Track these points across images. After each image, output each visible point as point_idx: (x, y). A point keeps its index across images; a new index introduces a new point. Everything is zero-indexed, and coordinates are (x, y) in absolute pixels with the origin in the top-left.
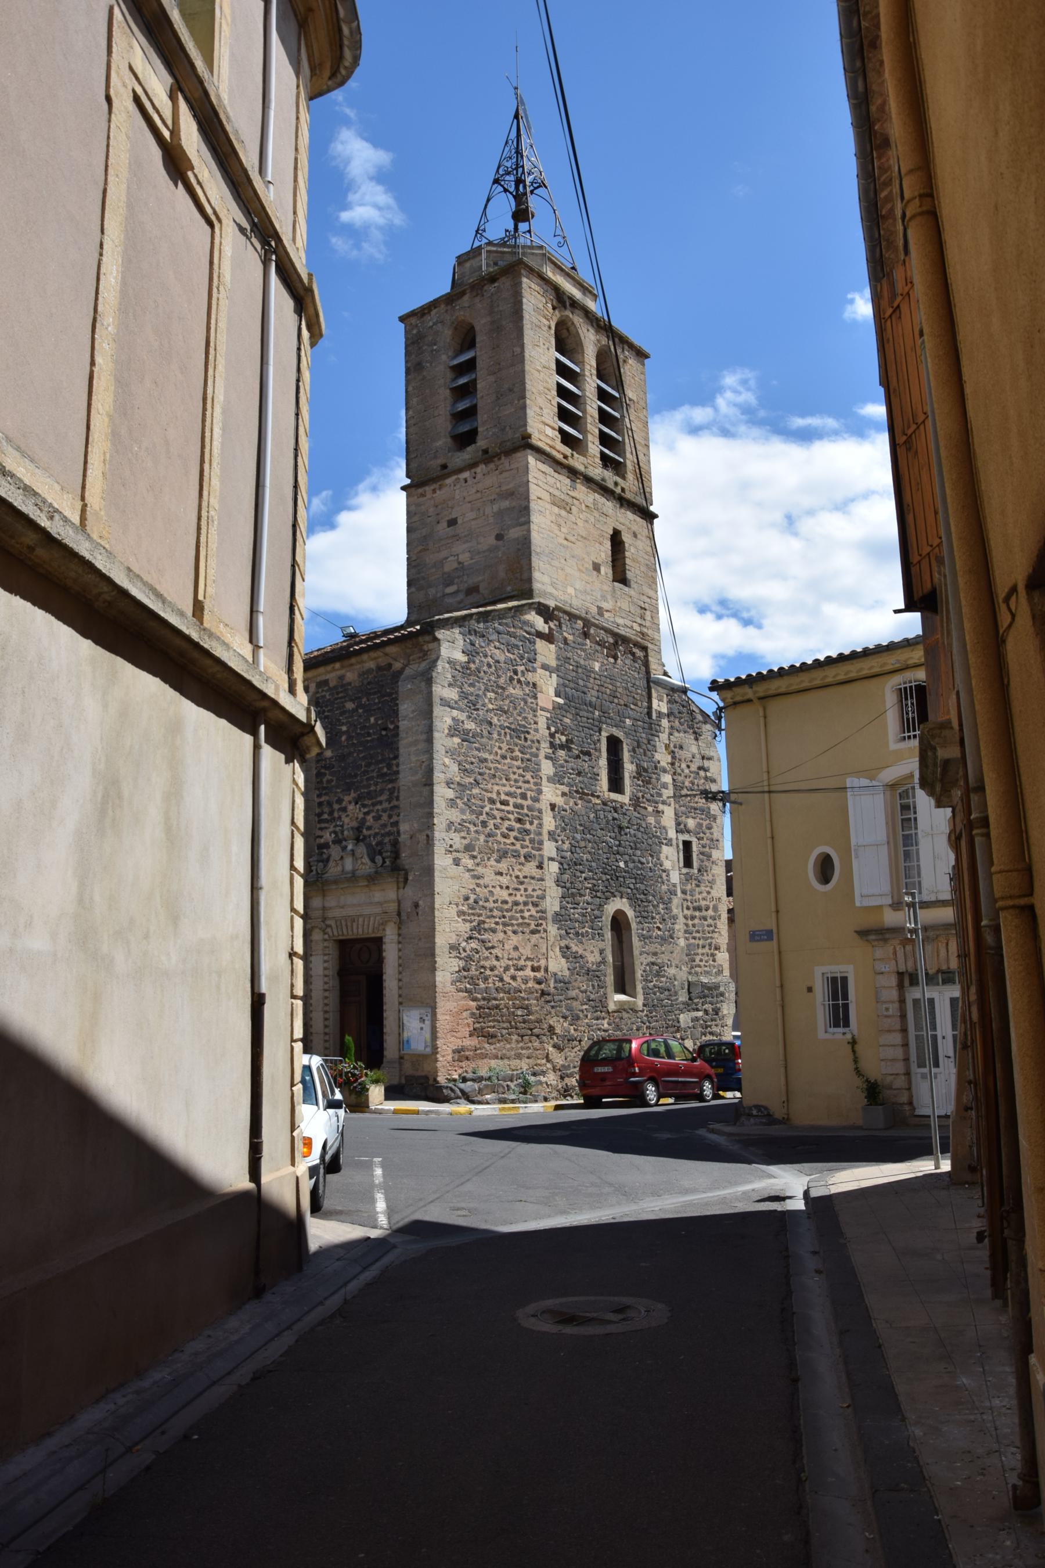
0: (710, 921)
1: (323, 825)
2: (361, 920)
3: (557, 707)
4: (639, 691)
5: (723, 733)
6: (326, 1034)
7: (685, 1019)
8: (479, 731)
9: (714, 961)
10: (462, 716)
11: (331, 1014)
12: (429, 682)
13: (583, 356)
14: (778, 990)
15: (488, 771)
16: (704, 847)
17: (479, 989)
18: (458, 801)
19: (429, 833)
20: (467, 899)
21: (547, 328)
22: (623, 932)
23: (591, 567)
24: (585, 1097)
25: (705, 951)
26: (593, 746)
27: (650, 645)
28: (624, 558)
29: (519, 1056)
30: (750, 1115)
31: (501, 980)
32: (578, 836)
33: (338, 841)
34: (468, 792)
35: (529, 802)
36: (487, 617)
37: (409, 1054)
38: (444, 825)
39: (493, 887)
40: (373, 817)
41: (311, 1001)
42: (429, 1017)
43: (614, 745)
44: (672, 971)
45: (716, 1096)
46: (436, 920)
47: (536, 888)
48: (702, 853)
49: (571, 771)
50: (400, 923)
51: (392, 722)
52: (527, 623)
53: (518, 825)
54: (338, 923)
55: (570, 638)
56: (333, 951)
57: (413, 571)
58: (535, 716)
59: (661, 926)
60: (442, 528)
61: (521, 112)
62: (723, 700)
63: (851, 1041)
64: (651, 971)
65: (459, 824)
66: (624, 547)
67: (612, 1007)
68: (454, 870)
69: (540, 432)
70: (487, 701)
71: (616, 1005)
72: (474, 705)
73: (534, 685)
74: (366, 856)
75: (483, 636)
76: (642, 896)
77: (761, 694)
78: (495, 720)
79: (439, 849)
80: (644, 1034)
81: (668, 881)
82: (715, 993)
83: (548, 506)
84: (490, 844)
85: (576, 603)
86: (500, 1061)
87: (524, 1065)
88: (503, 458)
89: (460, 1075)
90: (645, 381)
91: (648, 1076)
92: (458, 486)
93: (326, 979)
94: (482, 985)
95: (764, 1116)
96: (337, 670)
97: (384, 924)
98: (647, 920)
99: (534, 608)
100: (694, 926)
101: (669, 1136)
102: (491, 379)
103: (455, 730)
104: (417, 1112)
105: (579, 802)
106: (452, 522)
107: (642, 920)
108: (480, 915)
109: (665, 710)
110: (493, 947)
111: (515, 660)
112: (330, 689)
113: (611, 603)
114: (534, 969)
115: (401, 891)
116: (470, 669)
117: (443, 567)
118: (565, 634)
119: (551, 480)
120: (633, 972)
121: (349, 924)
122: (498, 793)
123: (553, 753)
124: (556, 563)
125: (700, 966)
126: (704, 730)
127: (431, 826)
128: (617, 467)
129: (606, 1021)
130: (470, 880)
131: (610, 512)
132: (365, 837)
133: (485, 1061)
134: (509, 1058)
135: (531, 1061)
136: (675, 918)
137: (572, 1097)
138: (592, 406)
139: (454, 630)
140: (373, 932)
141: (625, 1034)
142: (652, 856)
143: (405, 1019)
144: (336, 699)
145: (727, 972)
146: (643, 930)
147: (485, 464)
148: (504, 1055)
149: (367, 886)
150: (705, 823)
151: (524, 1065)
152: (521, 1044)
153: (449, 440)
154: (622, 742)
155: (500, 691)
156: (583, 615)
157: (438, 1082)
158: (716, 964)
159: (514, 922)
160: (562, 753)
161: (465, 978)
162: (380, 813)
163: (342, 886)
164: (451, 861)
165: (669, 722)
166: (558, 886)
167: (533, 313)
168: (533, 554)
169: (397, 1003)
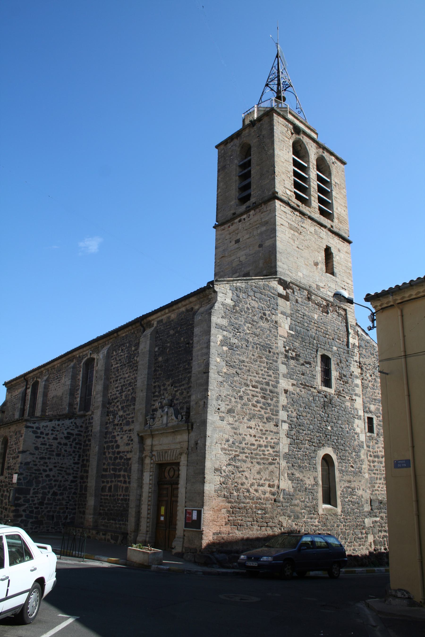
2: (169, 452)
4: (342, 333)
7: (368, 522)
10: (230, 335)
11: (152, 506)
12: (210, 314)
15: (245, 368)
18: (225, 383)
20: (228, 441)
23: (313, 264)
25: (380, 482)
26: (313, 360)
27: (348, 308)
28: (333, 261)
30: (396, 597)
31: (248, 491)
32: (301, 409)
33: (162, 407)
35: (271, 387)
39: (245, 435)
40: (179, 393)
43: (326, 360)
44: (360, 492)
47: (274, 437)
49: (299, 372)
53: (263, 400)
54: (159, 454)
55: (300, 300)
57: (218, 268)
59: (353, 465)
62: (375, 307)
64: (347, 491)
67: (321, 512)
70: (246, 328)
73: (276, 322)
74: (173, 415)
75: (245, 292)
76: (342, 447)
77: (399, 301)
78: (251, 340)
79: (211, 410)
81: (359, 439)
83: (288, 230)
84: (244, 410)
85: (303, 281)
88: (263, 206)
95: (406, 598)
96: (167, 313)
97: (181, 454)
98: (344, 461)
100: (374, 466)
103: (224, 342)
105: (303, 390)
108: (236, 451)
110: (243, 471)
114: (269, 486)
121: (163, 454)
125: (378, 490)
129: (317, 520)
131: (324, 237)
136: (362, 461)
138: (314, 184)
140: (175, 460)
144: (166, 329)
153: (237, 201)
154: (330, 359)
160: (292, 362)
162: (183, 391)
164: (218, 418)
168: (277, 253)
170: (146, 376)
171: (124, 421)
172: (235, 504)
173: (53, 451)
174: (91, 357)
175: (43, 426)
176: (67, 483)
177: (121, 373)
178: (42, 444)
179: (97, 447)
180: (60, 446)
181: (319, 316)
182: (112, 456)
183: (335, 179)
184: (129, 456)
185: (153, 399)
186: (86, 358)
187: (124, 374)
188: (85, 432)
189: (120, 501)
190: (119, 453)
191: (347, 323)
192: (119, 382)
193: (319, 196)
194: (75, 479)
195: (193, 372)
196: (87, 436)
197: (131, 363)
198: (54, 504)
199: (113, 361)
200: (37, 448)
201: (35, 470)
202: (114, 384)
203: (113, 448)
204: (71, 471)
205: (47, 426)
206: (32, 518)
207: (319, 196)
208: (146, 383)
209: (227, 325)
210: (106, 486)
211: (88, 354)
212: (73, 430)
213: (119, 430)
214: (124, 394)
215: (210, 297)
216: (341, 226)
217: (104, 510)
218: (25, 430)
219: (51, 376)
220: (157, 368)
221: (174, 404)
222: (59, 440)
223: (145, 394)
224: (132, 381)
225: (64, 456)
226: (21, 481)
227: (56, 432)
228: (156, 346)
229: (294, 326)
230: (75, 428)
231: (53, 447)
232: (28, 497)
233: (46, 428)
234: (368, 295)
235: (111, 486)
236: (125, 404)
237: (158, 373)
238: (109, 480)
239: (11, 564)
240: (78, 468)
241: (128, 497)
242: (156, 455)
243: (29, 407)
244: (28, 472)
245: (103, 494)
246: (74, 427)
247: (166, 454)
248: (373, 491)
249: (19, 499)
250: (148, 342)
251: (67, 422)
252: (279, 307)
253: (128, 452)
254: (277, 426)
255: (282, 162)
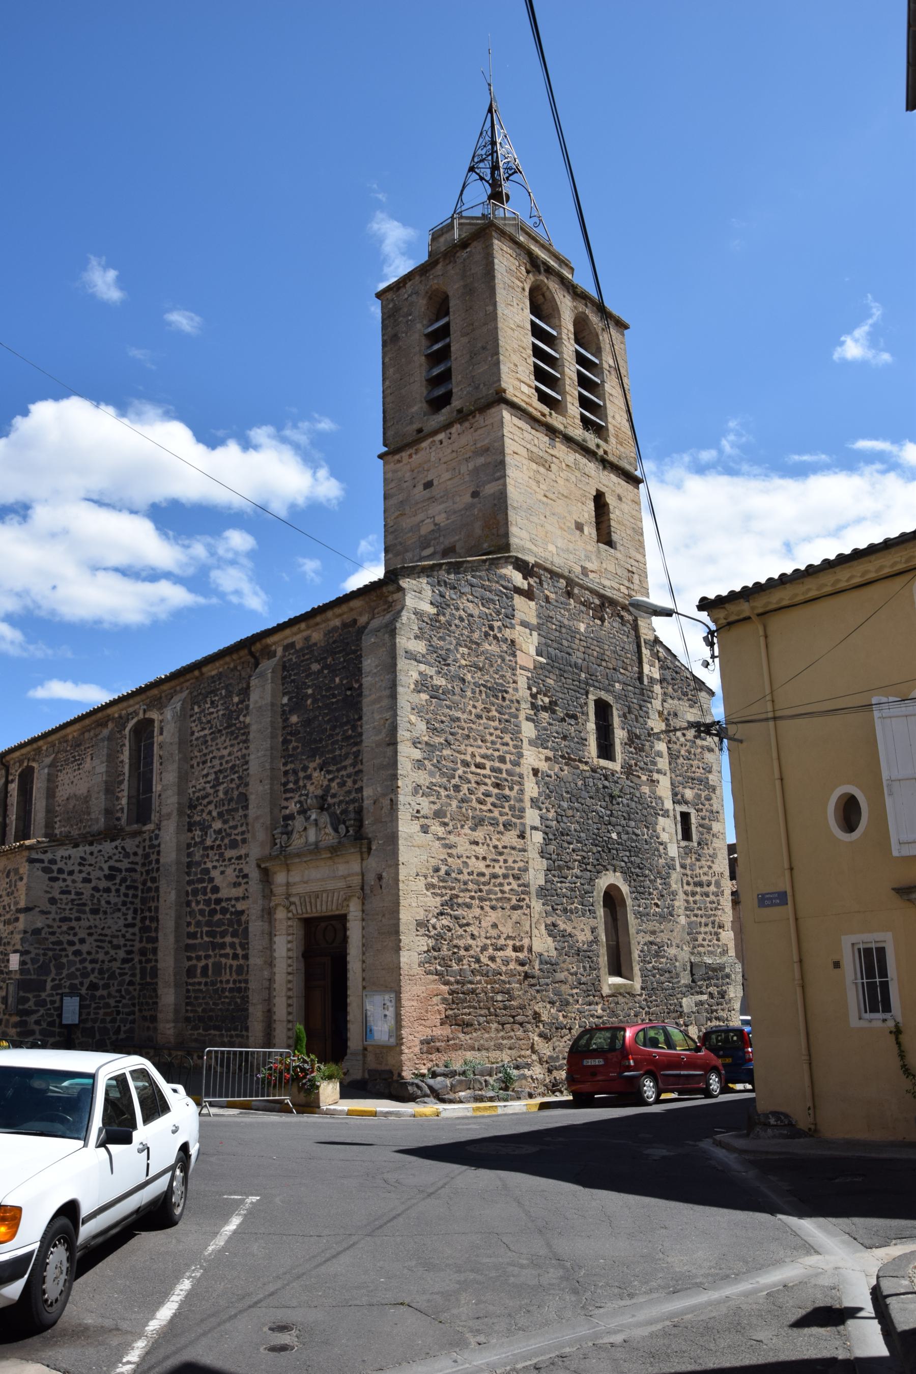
0: (712, 898)
1: (288, 795)
2: (324, 895)
3: (538, 667)
4: (629, 656)
5: (717, 660)
6: (289, 1021)
7: (688, 1003)
9: (718, 940)
10: (431, 671)
11: (295, 999)
12: (393, 633)
13: (560, 321)
14: (796, 967)
15: (460, 731)
16: (703, 819)
17: (452, 971)
18: (426, 762)
19: (393, 797)
20: (437, 870)
21: (519, 290)
22: (618, 908)
23: (573, 526)
24: (574, 1093)
25: (707, 929)
26: (579, 710)
28: (609, 520)
29: (499, 1047)
30: (767, 1125)
31: (478, 961)
32: (565, 805)
33: (303, 812)
34: (438, 753)
35: (509, 766)
36: (459, 568)
37: (373, 1046)
39: (467, 857)
40: (338, 784)
42: (393, 1004)
43: (603, 709)
44: (672, 951)
45: (725, 1090)
46: (401, 893)
47: (518, 859)
48: (702, 826)
50: (364, 898)
51: (357, 681)
52: (504, 577)
53: (496, 791)
55: (552, 596)
56: (298, 931)
57: (391, 537)
58: (514, 675)
59: (659, 903)
60: (419, 492)
61: (494, 106)
62: (714, 621)
63: (894, 1029)
64: (649, 951)
65: (428, 788)
66: (609, 508)
67: (606, 991)
68: (421, 838)
69: (515, 388)
70: (459, 656)
71: (610, 989)
72: (445, 660)
73: (513, 642)
74: (329, 826)
75: (455, 588)
76: (637, 870)
77: (760, 610)
78: (469, 677)
81: (666, 854)
82: (720, 974)
83: (526, 462)
84: (464, 810)
86: (477, 1053)
88: (478, 415)
89: (429, 1070)
90: (625, 350)
92: (434, 448)
93: (290, 961)
94: (456, 967)
95: (785, 1125)
96: (304, 630)
97: (347, 899)
99: (512, 563)
100: (695, 902)
101: (664, 1152)
102: (465, 340)
103: (422, 685)
104: (375, 1114)
105: (566, 768)
106: (428, 485)
107: (638, 896)
108: (452, 889)
109: (657, 676)
110: (468, 924)
111: (491, 615)
112: (297, 652)
113: (596, 563)
114: (516, 949)
116: (439, 621)
117: (419, 530)
120: (630, 953)
121: (313, 901)
122: (473, 755)
123: (535, 714)
125: (702, 946)
127: (395, 789)
129: (600, 1006)
130: (441, 849)
131: (593, 473)
132: (330, 806)
133: (459, 1052)
135: (513, 1052)
136: (674, 894)
137: (561, 1092)
138: (571, 370)
139: (421, 580)
140: (337, 909)
141: (621, 1021)
142: (647, 828)
143: (369, 1007)
144: (303, 661)
145: (732, 952)
146: (639, 906)
147: (460, 423)
149: (330, 858)
150: (703, 794)
151: (505, 1057)
152: (502, 1034)
153: (425, 405)
155: (474, 646)
156: (566, 574)
157: (403, 1078)
158: (720, 943)
159: (493, 897)
160: (545, 715)
161: (435, 958)
163: (305, 859)
164: (418, 828)
165: (662, 688)
166: (542, 857)
167: (505, 274)
168: (510, 508)
169: (361, 987)
170: (268, 753)
171: (226, 841)
172: (456, 986)
173: (84, 905)
174: (147, 716)
175: (62, 857)
176: (116, 965)
177: (213, 748)
178: (63, 892)
179: (173, 893)
180: (97, 895)
181: (588, 625)
182: (204, 907)
184: (240, 906)
185: (284, 796)
186: (135, 720)
187: (218, 749)
188: (144, 865)
189: (227, 994)
190: (218, 901)
191: (638, 637)
192: (209, 764)
193: (580, 394)
195: (364, 744)
196: (148, 872)
197: (233, 728)
198: (93, 1005)
199: (193, 725)
200: (53, 901)
201: (53, 943)
202: (199, 768)
203: (205, 894)
204: (122, 941)
205: (70, 857)
206: (54, 1036)
207: (580, 394)
208: (268, 766)
209: (424, 651)
210: (195, 966)
211: (139, 709)
212: (121, 861)
213: (217, 857)
214: (221, 788)
215: (390, 599)
216: (622, 449)
218: (27, 867)
220: (289, 737)
222: (93, 884)
224: (238, 762)
225: (105, 913)
226: (26, 967)
228: (284, 694)
229: (544, 648)
231: (84, 896)
233: (67, 861)
235: (207, 965)
236: (226, 808)
238: (202, 953)
239: (146, 1120)
240: (134, 934)
241: (243, 985)
242: (298, 903)
243: (17, 819)
244: (39, 948)
245: (191, 981)
248: (694, 947)
249: (26, 1000)
250: (269, 687)
251: (108, 847)
253: (237, 899)
255: (512, 329)
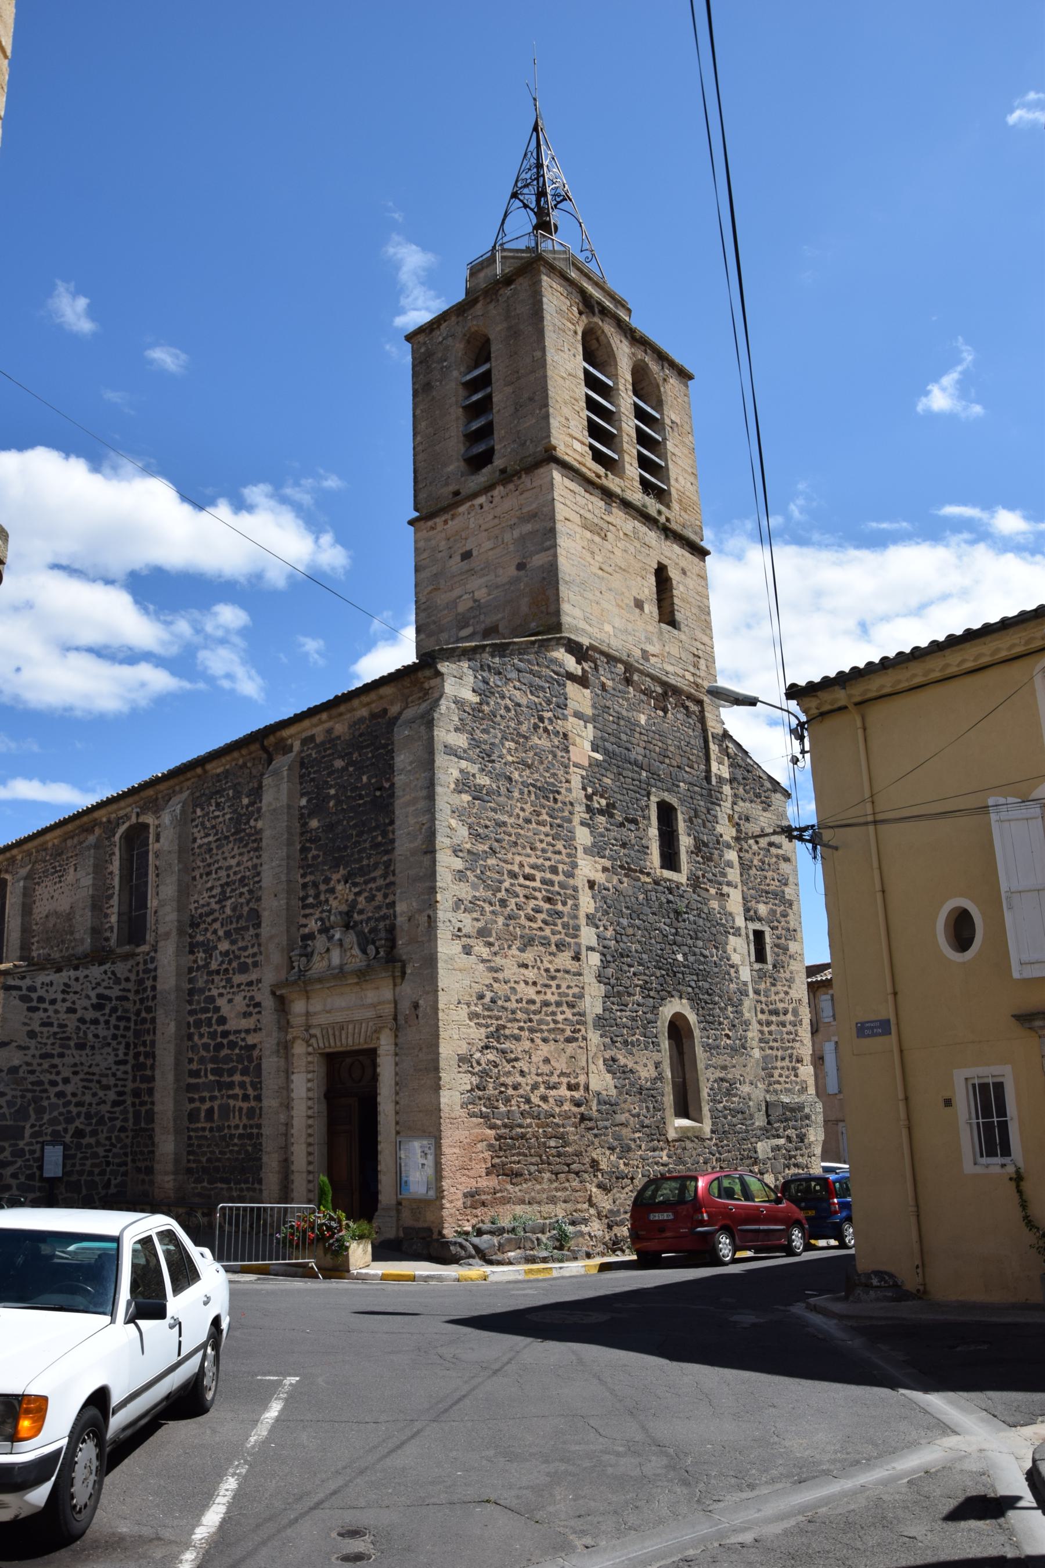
0: (789, 1028)
2: (351, 1027)
3: (594, 764)
4: (695, 752)
5: (808, 756)
6: (309, 1172)
7: (763, 1148)
8: (495, 787)
9: (796, 1076)
10: (473, 769)
12: (430, 724)
13: (616, 369)
14: (902, 1106)
15: (507, 838)
16: (779, 938)
17: (499, 1113)
18: (468, 873)
19: (431, 913)
20: (481, 997)
21: (571, 333)
22: (684, 1040)
23: (632, 604)
24: (639, 1253)
26: (640, 813)
28: (672, 596)
29: (553, 1200)
30: (868, 1286)
31: (528, 1101)
32: (625, 922)
33: (325, 930)
34: (481, 862)
35: (561, 877)
36: (504, 651)
38: (450, 904)
39: (515, 982)
41: (293, 1131)
42: (432, 1150)
43: (666, 812)
44: (745, 1089)
46: (441, 1024)
47: (572, 984)
48: (777, 946)
49: (614, 842)
50: (397, 1029)
51: (388, 780)
52: (555, 661)
53: (547, 906)
54: (324, 1032)
55: (609, 683)
56: (320, 1068)
57: (423, 615)
58: (567, 773)
59: (730, 1034)
60: (455, 564)
62: (805, 711)
63: (1014, 1176)
65: (471, 902)
67: (672, 1135)
70: (505, 751)
71: (677, 1133)
72: (489, 756)
73: (565, 736)
74: (356, 946)
75: (500, 673)
76: (706, 997)
77: (858, 699)
78: (516, 776)
80: (713, 1168)
81: (738, 978)
82: (799, 1115)
83: (579, 530)
84: (511, 928)
86: (527, 1207)
87: (559, 1211)
88: (524, 476)
89: (473, 1227)
90: (689, 404)
91: (720, 1224)
92: (473, 514)
93: (310, 1103)
94: (503, 1109)
95: (889, 1286)
97: (378, 1031)
99: (564, 645)
100: (770, 1033)
102: (509, 390)
103: (463, 785)
104: (413, 1278)
105: (625, 880)
106: (467, 555)
107: (707, 1026)
108: (498, 1018)
109: (726, 775)
110: (516, 1059)
111: (541, 704)
112: (317, 746)
113: (657, 646)
114: (571, 1087)
115: (398, 989)
116: (483, 712)
117: (456, 607)
118: (602, 678)
119: (582, 501)
120: (698, 1091)
121: (337, 1033)
122: (521, 865)
123: (591, 818)
124: (589, 595)
125: (779, 1083)
126: (773, 799)
127: (433, 904)
128: (661, 495)
129: (665, 1152)
131: (654, 543)
133: (508, 1206)
134: (539, 1203)
136: (747, 1023)
137: (623, 1251)
138: (629, 425)
139: (461, 664)
141: (689, 1169)
142: (716, 948)
144: (324, 757)
145: (812, 1090)
146: (708, 1038)
148: (533, 1198)
149: (357, 984)
151: (559, 1211)
152: (555, 1184)
153: (462, 464)
155: (521, 740)
156: (625, 658)
157: (444, 1236)
158: (798, 1080)
159: (544, 1027)
160: (601, 819)
161: (480, 1099)
163: (328, 985)
164: (459, 949)
165: (732, 788)
169: (394, 1132)
170: (284, 863)
171: (235, 964)
173: (69, 1038)
174: (140, 820)
175: (43, 983)
176: (105, 1108)
177: (219, 857)
178: (43, 1024)
179: (173, 1024)
180: (83, 1027)
182: (209, 1041)
183: (671, 414)
184: (251, 1040)
185: (303, 912)
187: (225, 859)
188: (137, 992)
189: (236, 1141)
190: (225, 1034)
191: (705, 730)
192: (214, 876)
193: (639, 453)
194: (121, 1098)
195: (397, 852)
196: (142, 1001)
197: (242, 834)
198: (79, 1155)
199: (195, 830)
200: (32, 1035)
201: (33, 1084)
203: (210, 1025)
204: (112, 1081)
205: (52, 984)
207: (639, 453)
208: (284, 878)
209: (465, 745)
210: (198, 1109)
212: (111, 988)
213: (223, 983)
214: (229, 903)
215: (426, 685)
216: (686, 517)
217: (199, 1161)
219: (37, 866)
220: (308, 845)
221: (355, 922)
222: (78, 1015)
223: (283, 902)
224: (248, 873)
225: (93, 1048)
227: (71, 995)
228: (302, 795)
230: (114, 983)
231: (68, 1029)
232: (21, 1144)
233: (49, 988)
234: (793, 686)
236: (234, 926)
237: (310, 856)
238: (206, 1094)
240: (126, 1072)
241: (255, 1131)
242: (319, 1035)
244: (15, 1090)
245: (193, 1126)
246: (111, 981)
247: (344, 1032)
248: (770, 1084)
250: (284, 787)
251: (96, 972)
252: (569, 702)
254: (579, 960)
